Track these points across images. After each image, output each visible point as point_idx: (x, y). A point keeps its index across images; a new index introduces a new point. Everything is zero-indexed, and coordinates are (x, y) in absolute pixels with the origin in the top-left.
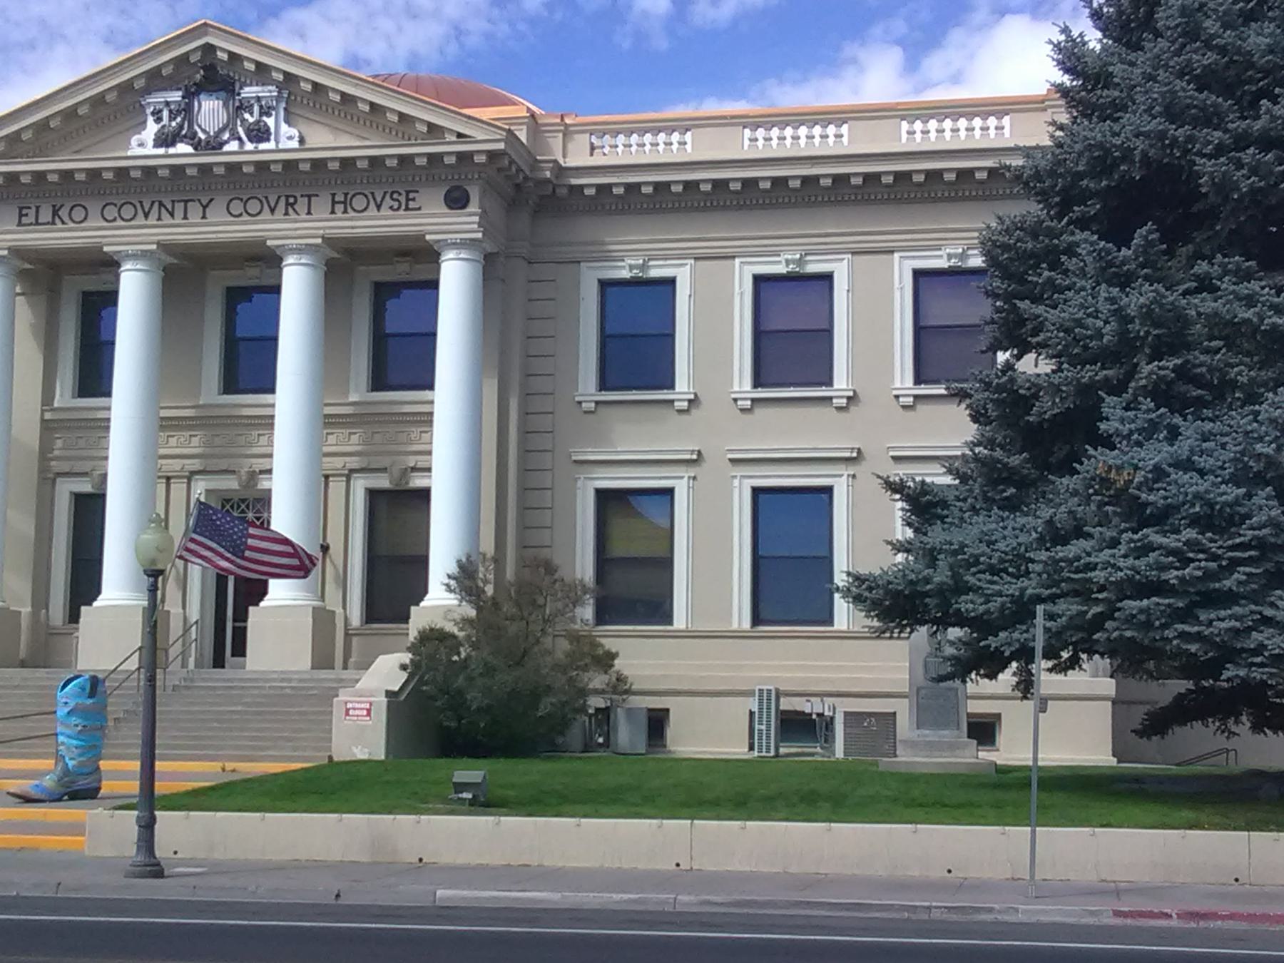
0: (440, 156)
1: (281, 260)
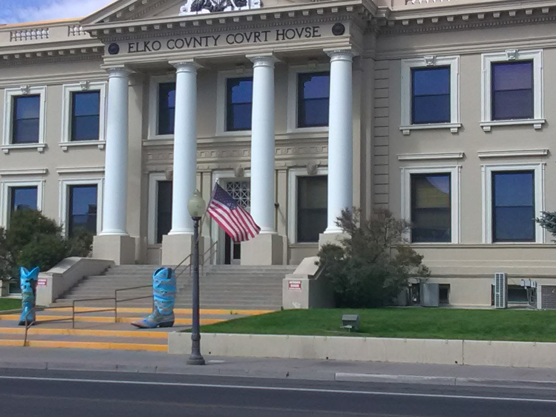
1: (253, 64)
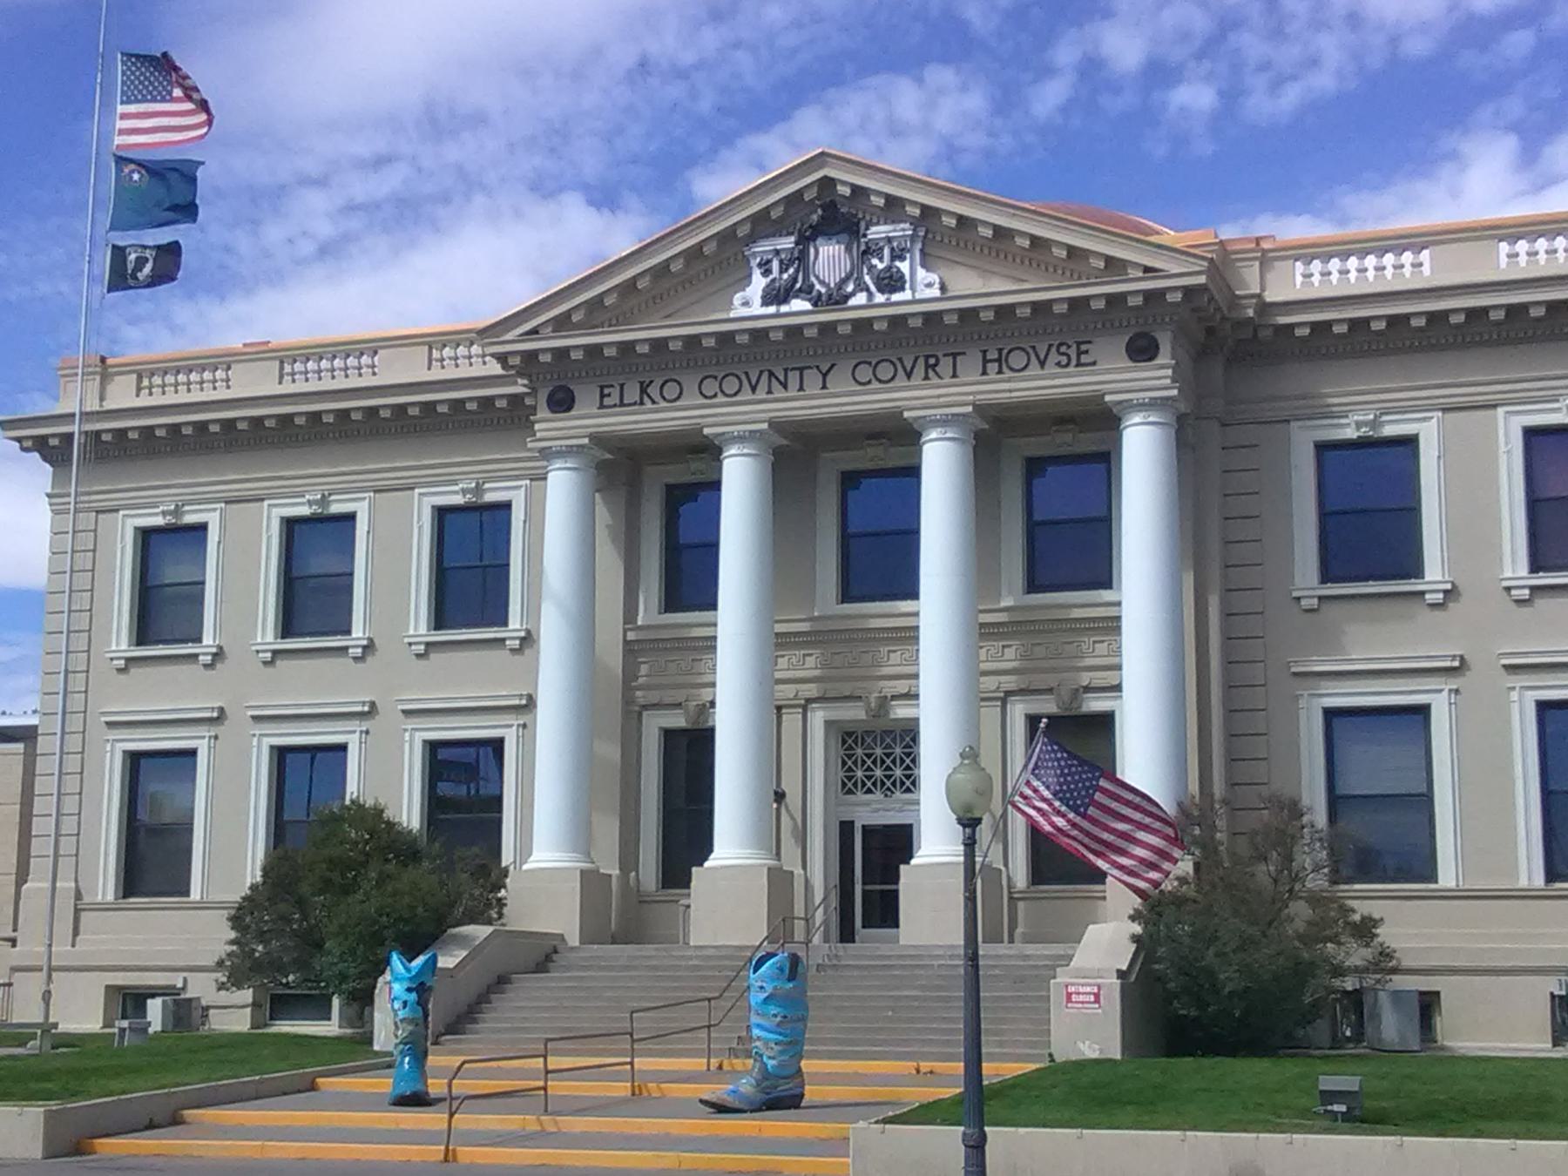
0: (1122, 297)
